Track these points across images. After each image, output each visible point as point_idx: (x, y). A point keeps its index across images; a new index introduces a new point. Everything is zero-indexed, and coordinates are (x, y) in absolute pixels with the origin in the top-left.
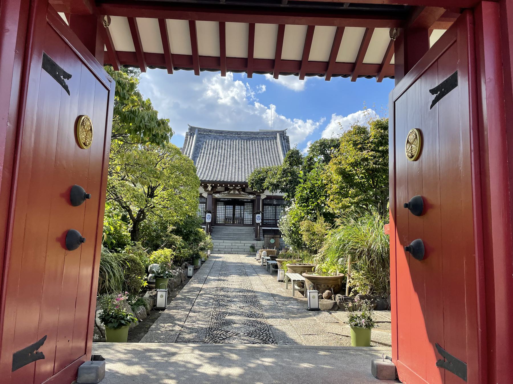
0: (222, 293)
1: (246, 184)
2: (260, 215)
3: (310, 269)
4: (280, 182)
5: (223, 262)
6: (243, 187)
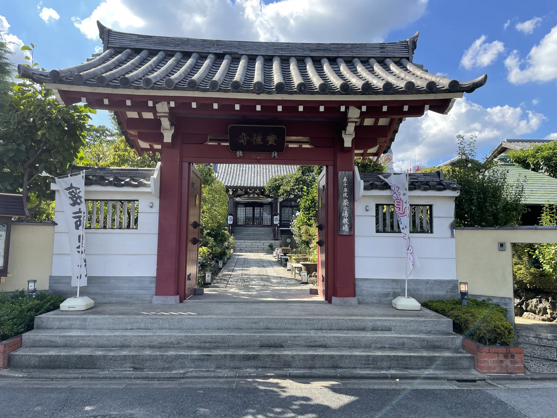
0: (246, 276)
1: (263, 188)
2: (278, 217)
3: (306, 260)
4: (293, 189)
5: (245, 259)
6: (261, 191)
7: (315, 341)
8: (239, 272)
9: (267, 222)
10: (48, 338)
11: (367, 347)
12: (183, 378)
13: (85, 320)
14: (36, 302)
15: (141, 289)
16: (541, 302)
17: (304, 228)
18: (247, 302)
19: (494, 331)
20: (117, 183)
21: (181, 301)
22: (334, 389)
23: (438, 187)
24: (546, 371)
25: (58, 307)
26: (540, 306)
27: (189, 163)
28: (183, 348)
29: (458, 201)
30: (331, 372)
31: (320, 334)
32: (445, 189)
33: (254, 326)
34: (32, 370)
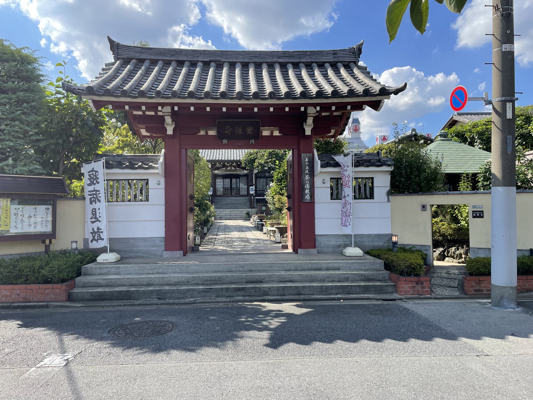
1: (239, 161)
2: (254, 187)
3: (280, 224)
4: (267, 163)
5: (225, 225)
7: (285, 278)
8: (222, 236)
9: (243, 192)
10: (94, 281)
11: (323, 281)
12: (194, 303)
13: (119, 268)
14: (80, 256)
15: (154, 246)
16: (458, 250)
17: (277, 197)
18: (234, 254)
19: (408, 267)
20: (132, 166)
21: (184, 255)
22: (298, 306)
23: (377, 163)
24: (447, 294)
25: (95, 260)
26: (458, 252)
27: (186, 150)
28: (191, 285)
29: (392, 173)
30: (297, 297)
31: (288, 273)
32: (382, 165)
33: (241, 269)
34: (86, 302)
